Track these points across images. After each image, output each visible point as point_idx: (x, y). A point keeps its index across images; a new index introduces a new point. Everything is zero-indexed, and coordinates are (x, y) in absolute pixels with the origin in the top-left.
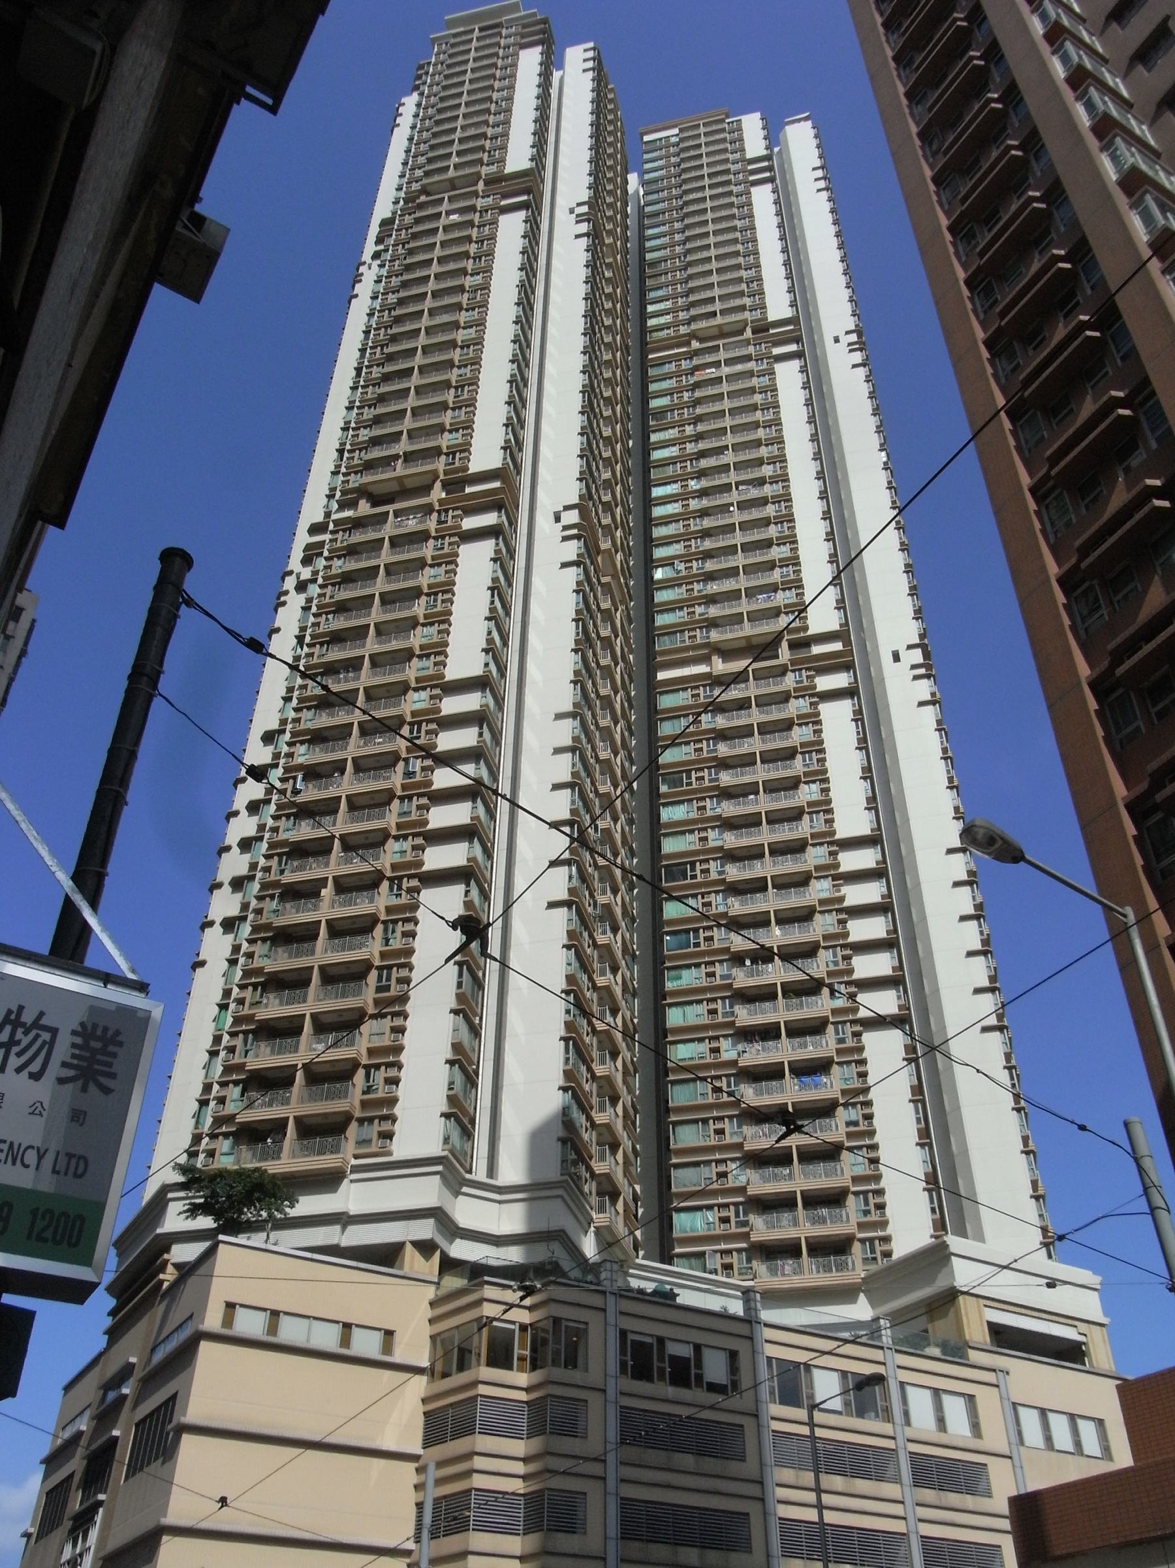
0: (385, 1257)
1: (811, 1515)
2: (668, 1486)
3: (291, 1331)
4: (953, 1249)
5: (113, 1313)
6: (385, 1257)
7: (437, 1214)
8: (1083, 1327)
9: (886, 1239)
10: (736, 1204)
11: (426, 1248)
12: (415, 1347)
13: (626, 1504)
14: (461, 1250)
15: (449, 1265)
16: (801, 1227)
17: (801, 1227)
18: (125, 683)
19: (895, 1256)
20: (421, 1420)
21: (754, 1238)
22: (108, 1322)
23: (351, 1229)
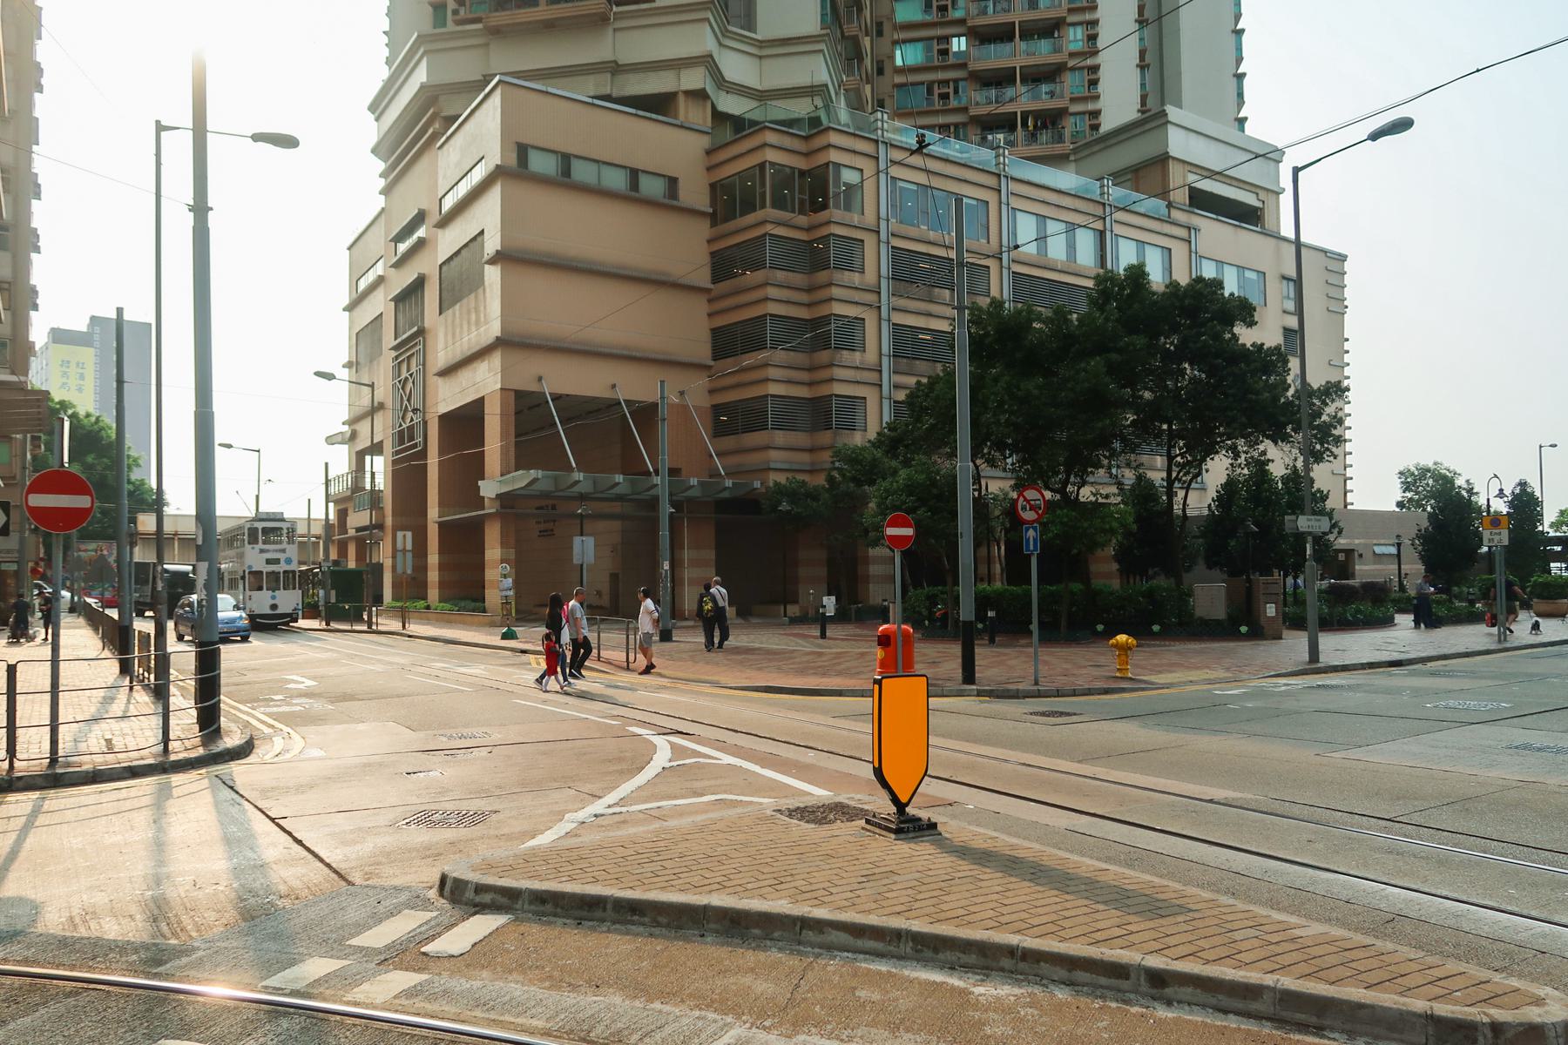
0: (658, 105)
1: (409, 556)
2: (930, 315)
3: (582, 172)
4: (1170, 118)
5: (383, 175)
6: (658, 105)
7: (707, 61)
8: (1262, 195)
9: (1096, 114)
10: (956, 81)
11: (699, 95)
12: (695, 193)
13: (897, 328)
14: (732, 105)
15: (719, 117)
16: (1022, 100)
17: (1022, 100)
18: (43, 52)
19: (1104, 129)
20: (707, 259)
21: (973, 112)
22: (382, 183)
23: (621, 78)
